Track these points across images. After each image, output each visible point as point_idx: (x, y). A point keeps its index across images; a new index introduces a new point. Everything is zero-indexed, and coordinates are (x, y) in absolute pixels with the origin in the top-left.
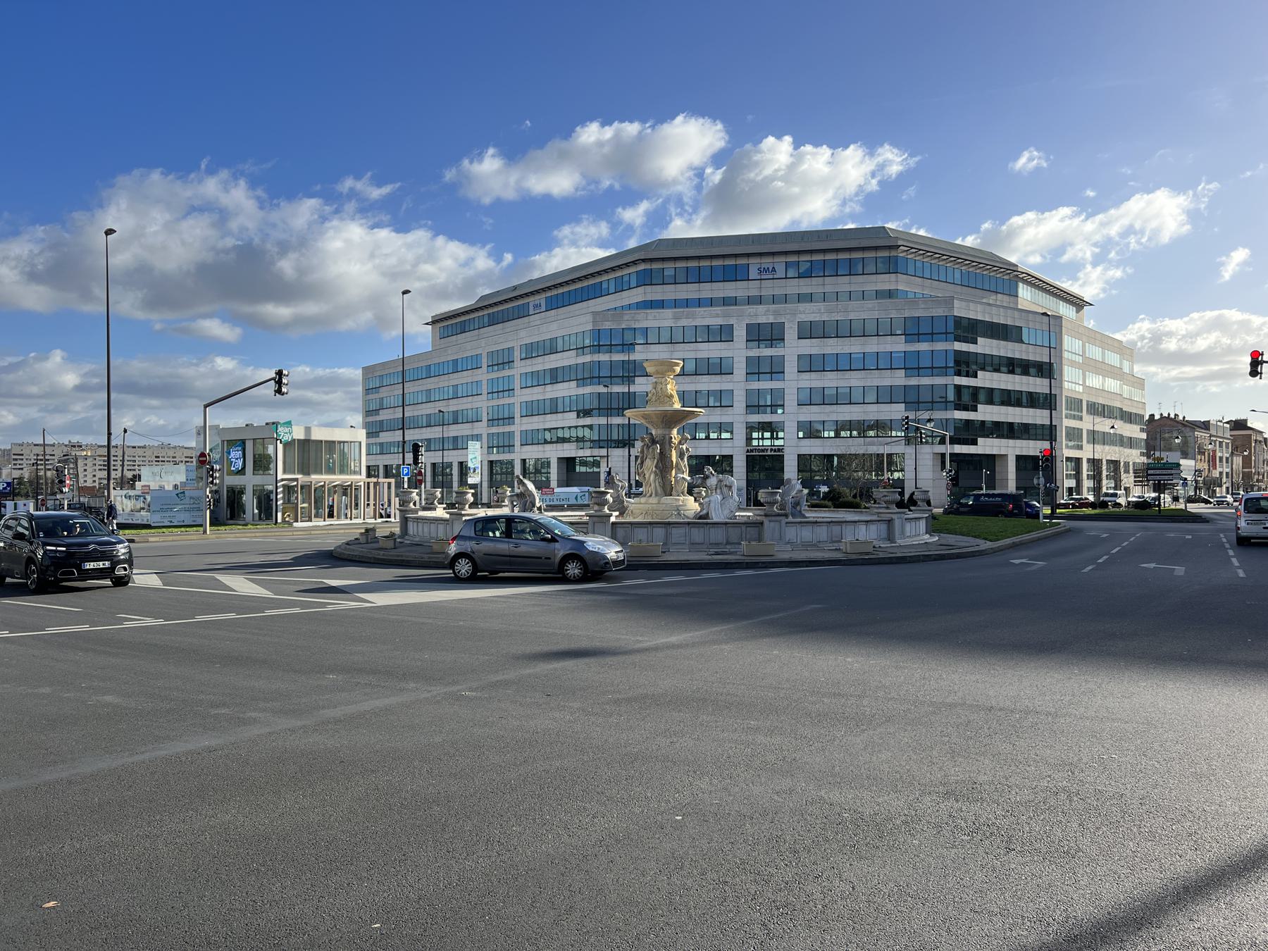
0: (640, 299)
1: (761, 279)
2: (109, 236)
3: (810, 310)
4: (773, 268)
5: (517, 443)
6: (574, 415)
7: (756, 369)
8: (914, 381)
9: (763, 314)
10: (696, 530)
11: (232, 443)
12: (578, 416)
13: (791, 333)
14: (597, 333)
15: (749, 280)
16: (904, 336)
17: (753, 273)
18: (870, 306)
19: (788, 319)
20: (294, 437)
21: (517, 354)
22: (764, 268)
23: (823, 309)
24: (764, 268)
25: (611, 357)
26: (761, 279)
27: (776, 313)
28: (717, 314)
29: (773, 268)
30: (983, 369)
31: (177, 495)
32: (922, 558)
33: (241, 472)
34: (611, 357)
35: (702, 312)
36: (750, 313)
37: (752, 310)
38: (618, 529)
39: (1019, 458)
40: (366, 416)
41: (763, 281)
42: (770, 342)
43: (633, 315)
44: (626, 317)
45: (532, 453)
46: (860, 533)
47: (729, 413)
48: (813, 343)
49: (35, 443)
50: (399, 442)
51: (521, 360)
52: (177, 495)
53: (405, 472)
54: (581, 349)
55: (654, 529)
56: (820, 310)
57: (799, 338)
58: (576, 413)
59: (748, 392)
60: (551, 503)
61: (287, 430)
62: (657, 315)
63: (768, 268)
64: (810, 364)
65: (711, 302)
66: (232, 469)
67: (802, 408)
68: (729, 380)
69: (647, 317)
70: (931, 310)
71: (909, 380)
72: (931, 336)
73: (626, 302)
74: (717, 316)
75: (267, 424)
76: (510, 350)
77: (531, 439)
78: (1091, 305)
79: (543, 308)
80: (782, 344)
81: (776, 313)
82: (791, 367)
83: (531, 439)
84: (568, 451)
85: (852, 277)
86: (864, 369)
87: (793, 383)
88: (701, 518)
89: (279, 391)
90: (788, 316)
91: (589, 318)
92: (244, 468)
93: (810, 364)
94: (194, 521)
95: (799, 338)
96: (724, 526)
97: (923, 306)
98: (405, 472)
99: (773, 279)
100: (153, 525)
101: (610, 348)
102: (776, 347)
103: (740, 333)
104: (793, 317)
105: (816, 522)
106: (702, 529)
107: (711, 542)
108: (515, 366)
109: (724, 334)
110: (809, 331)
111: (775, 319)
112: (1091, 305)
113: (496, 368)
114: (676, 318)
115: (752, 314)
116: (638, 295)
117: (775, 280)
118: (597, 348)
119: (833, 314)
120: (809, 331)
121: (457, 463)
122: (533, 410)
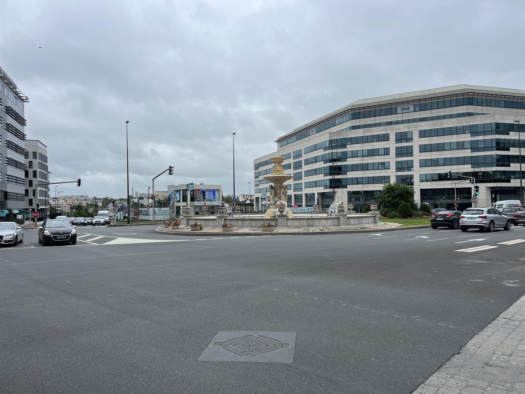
0: (350, 125)
1: (403, 113)
2: (127, 123)
3: (424, 125)
4: (408, 107)
5: (303, 187)
6: (323, 175)
7: (400, 152)
8: (475, 154)
9: (402, 128)
10: (253, 221)
11: (177, 191)
12: (324, 176)
13: (416, 136)
14: (331, 142)
15: (397, 114)
16: (470, 134)
17: (399, 111)
18: (453, 121)
19: (414, 129)
20: (194, 189)
21: (303, 152)
22: (404, 108)
23: (430, 124)
24: (404, 108)
25: (337, 151)
26: (403, 113)
27: (409, 127)
28: (382, 129)
29: (408, 107)
30: (514, 147)
31: (158, 209)
32: (327, 233)
33: (179, 201)
34: (337, 151)
35: (376, 129)
36: (397, 128)
37: (397, 127)
38: (227, 221)
39: (191, 202)
40: (255, 178)
41: (404, 114)
42: (406, 140)
43: (346, 133)
44: (343, 134)
45: (309, 191)
46: (323, 223)
47: (388, 172)
48: (426, 139)
49: (162, 191)
50: (267, 188)
51: (304, 154)
52: (158, 209)
53: (234, 200)
54: (325, 149)
55: (239, 221)
56: (429, 124)
57: (419, 138)
58: (323, 174)
59: (397, 162)
60: (294, 211)
61: (192, 186)
62: (356, 132)
63: (406, 108)
64: (423, 149)
65: (380, 125)
66: (177, 200)
67: (422, 168)
68: (388, 158)
69: (352, 133)
70: (483, 121)
71: (473, 154)
72: (484, 133)
73: (345, 127)
74: (382, 130)
75: (201, 184)
76: (301, 150)
77: (310, 185)
78: (275, 142)
79: (315, 133)
80: (412, 141)
81: (409, 127)
82: (416, 150)
83: (310, 185)
84: (318, 190)
85: (445, 108)
86: (451, 150)
87: (417, 157)
88: (273, 217)
89: (170, 174)
90: (414, 128)
91: (328, 135)
92: (180, 200)
93: (423, 149)
94: (164, 219)
95: (419, 138)
96: (263, 220)
97: (479, 119)
98: (234, 200)
99: (408, 112)
100: (150, 220)
101: (337, 147)
102: (409, 142)
103: (392, 137)
104: (415, 129)
105: (300, 219)
106: (255, 221)
107: (258, 226)
108: (302, 157)
109: (385, 138)
110: (423, 134)
111: (408, 130)
112: (275, 142)
113: (296, 157)
114: (364, 132)
115: (398, 128)
116: (350, 124)
117: (409, 113)
118: (331, 147)
119: (435, 126)
120: (423, 134)
121: (304, 194)
122: (308, 173)
